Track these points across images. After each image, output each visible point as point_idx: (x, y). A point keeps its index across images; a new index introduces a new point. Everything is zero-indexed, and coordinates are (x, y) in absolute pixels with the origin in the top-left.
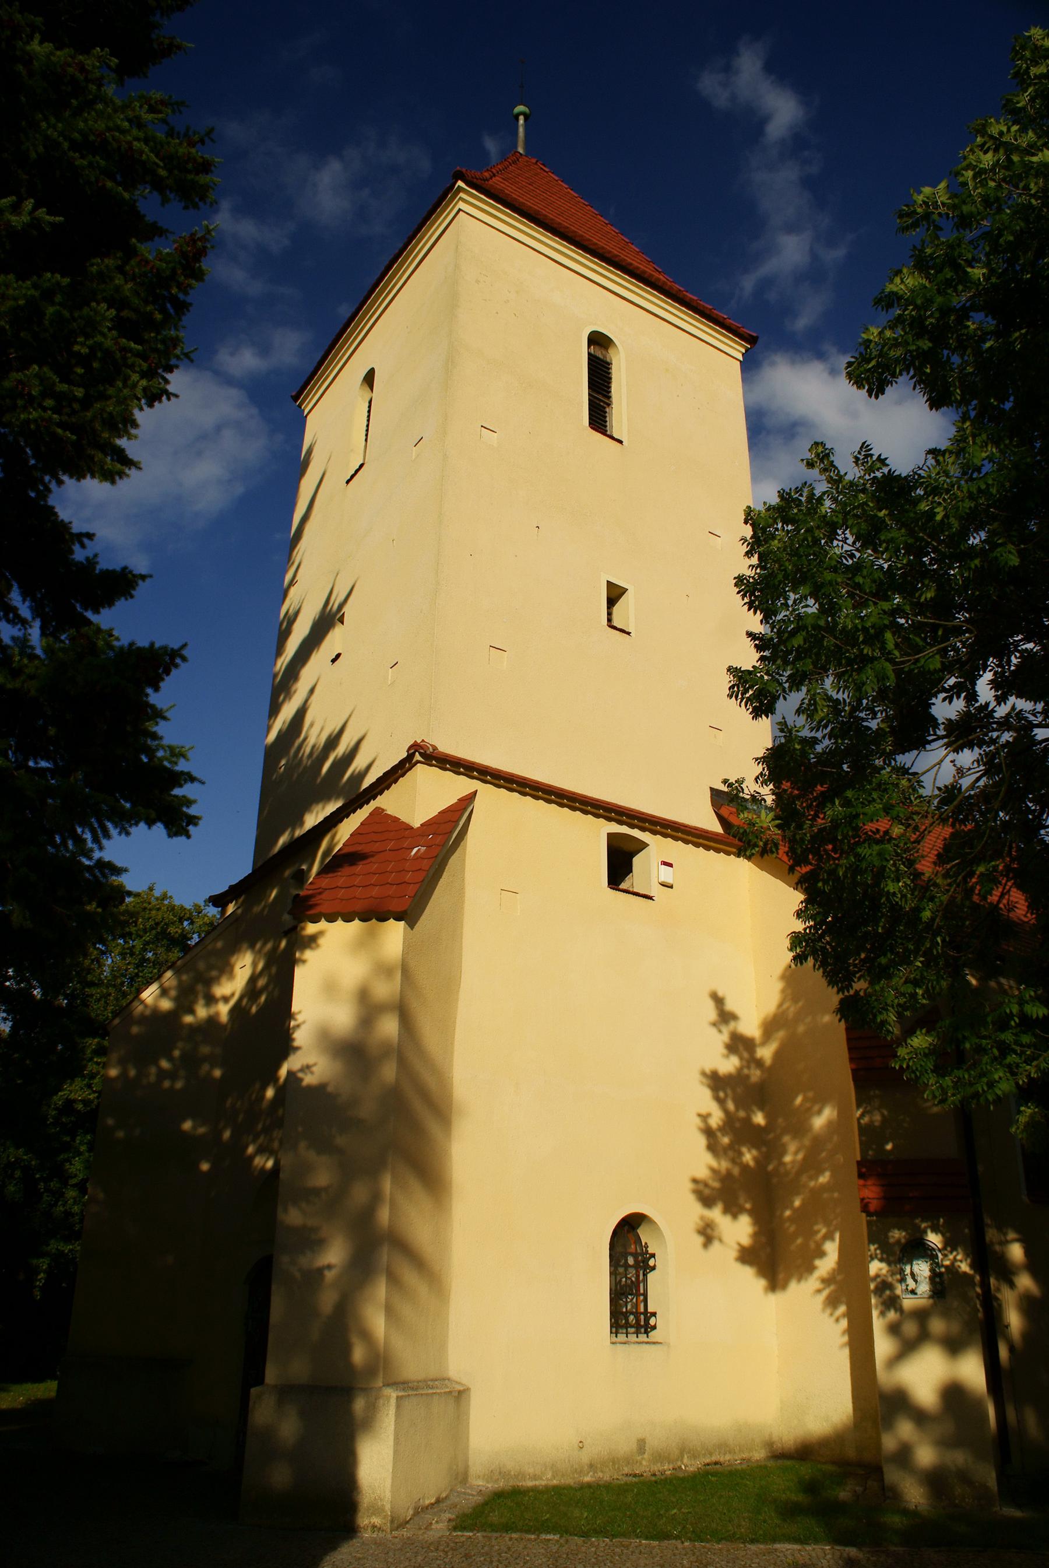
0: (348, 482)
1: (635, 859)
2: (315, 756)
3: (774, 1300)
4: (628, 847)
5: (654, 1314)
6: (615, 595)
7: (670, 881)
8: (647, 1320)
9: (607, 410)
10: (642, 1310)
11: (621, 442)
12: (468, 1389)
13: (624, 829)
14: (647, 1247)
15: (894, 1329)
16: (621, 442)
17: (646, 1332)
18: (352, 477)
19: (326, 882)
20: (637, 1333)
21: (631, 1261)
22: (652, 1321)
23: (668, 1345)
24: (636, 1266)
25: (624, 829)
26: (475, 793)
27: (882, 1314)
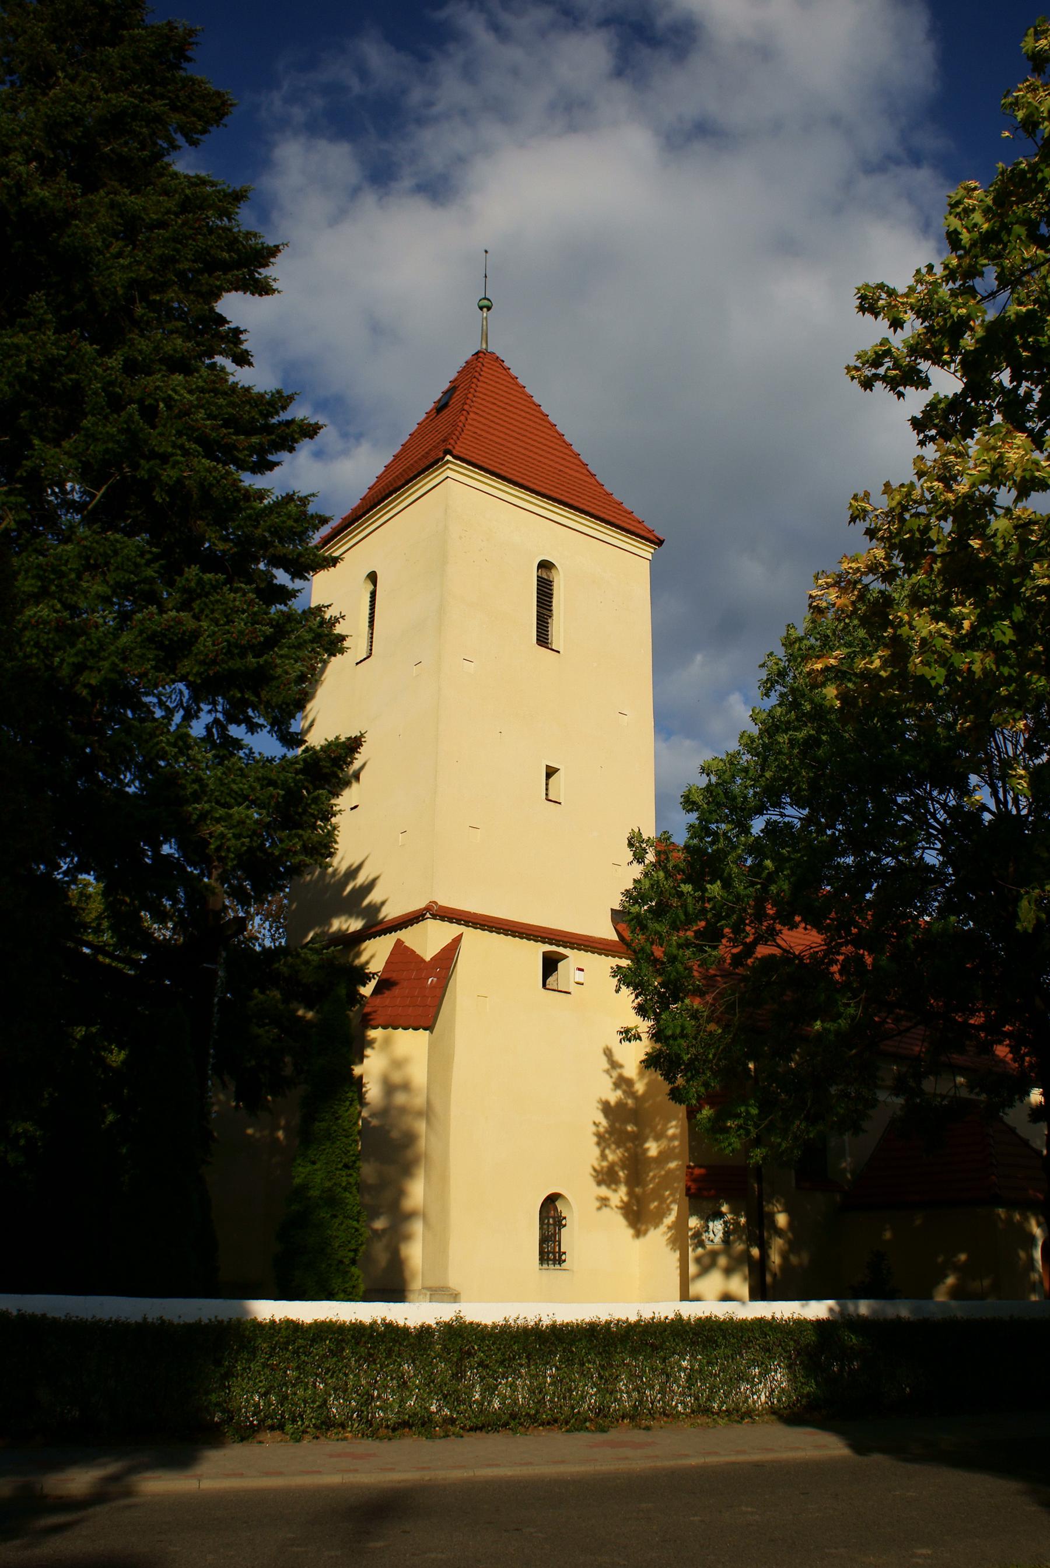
0: (357, 664)
1: (559, 964)
2: (337, 878)
3: (639, 1243)
4: (555, 957)
5: (565, 1253)
6: (550, 772)
7: (581, 981)
8: (560, 1256)
9: (549, 621)
10: (557, 1250)
11: (559, 652)
12: (459, 1294)
13: (554, 948)
14: (561, 1212)
15: (698, 1260)
16: (559, 652)
17: (560, 1264)
18: (361, 661)
19: (378, 1000)
20: (554, 1264)
21: (551, 1221)
22: (563, 1257)
23: (573, 1271)
24: (554, 1224)
25: (554, 948)
26: (462, 934)
27: (694, 1250)
